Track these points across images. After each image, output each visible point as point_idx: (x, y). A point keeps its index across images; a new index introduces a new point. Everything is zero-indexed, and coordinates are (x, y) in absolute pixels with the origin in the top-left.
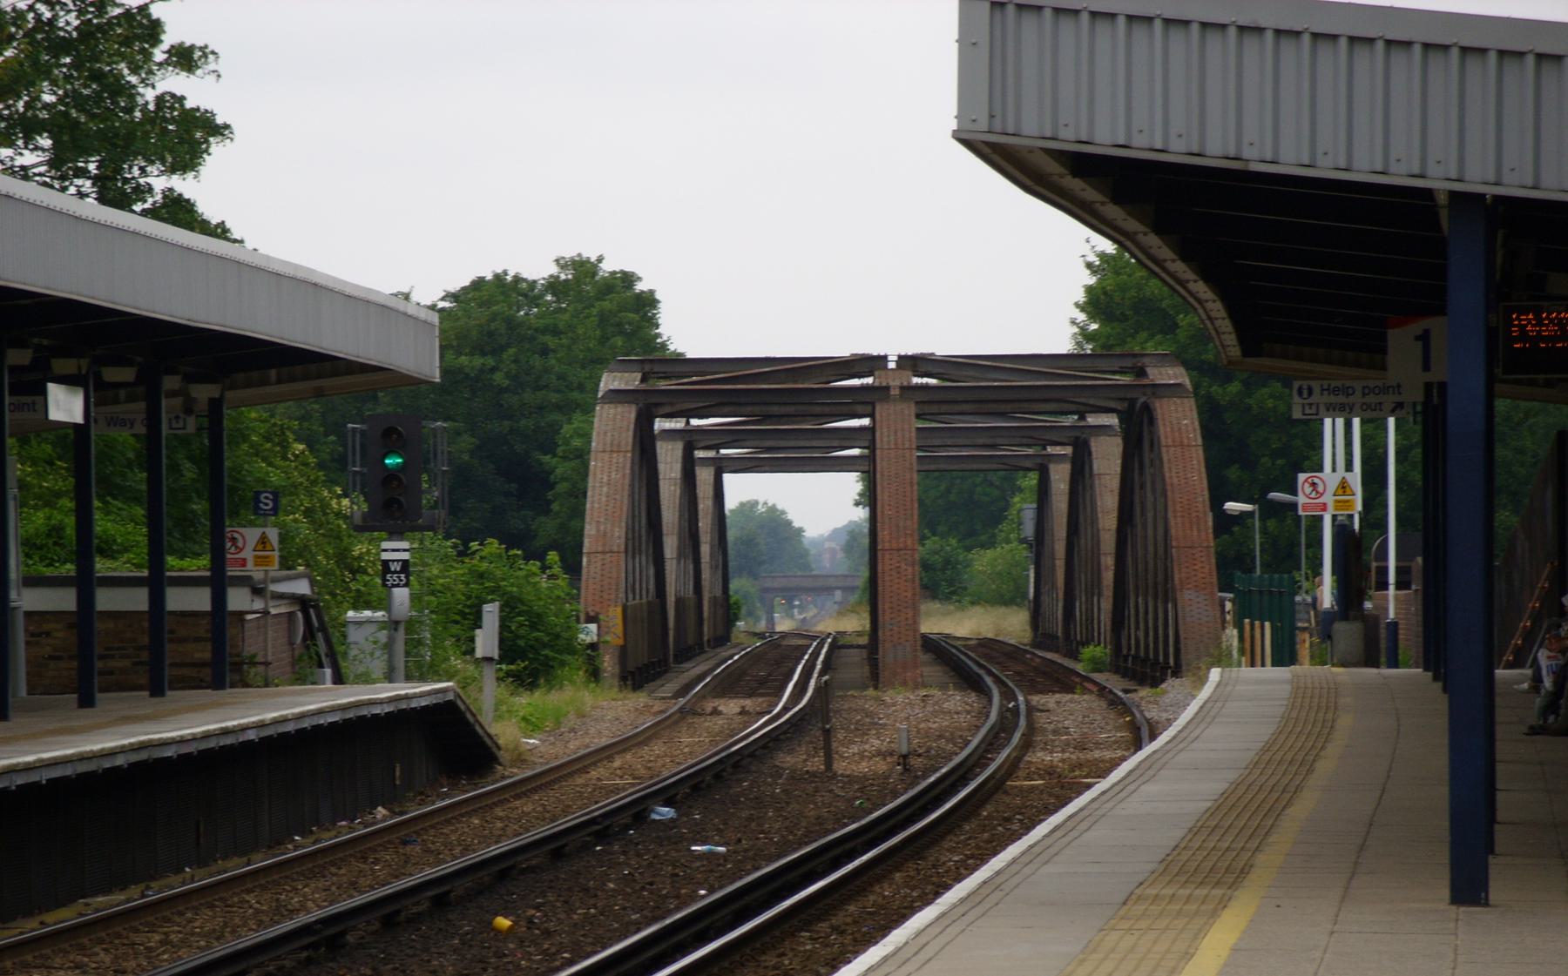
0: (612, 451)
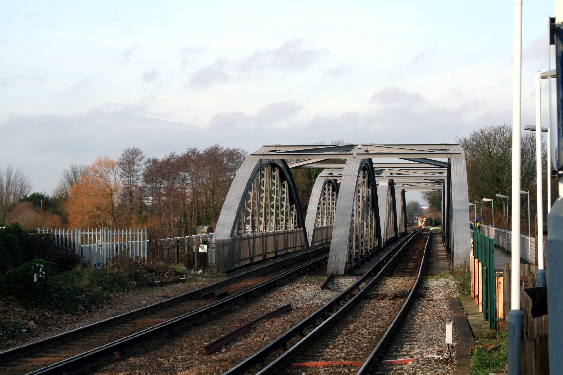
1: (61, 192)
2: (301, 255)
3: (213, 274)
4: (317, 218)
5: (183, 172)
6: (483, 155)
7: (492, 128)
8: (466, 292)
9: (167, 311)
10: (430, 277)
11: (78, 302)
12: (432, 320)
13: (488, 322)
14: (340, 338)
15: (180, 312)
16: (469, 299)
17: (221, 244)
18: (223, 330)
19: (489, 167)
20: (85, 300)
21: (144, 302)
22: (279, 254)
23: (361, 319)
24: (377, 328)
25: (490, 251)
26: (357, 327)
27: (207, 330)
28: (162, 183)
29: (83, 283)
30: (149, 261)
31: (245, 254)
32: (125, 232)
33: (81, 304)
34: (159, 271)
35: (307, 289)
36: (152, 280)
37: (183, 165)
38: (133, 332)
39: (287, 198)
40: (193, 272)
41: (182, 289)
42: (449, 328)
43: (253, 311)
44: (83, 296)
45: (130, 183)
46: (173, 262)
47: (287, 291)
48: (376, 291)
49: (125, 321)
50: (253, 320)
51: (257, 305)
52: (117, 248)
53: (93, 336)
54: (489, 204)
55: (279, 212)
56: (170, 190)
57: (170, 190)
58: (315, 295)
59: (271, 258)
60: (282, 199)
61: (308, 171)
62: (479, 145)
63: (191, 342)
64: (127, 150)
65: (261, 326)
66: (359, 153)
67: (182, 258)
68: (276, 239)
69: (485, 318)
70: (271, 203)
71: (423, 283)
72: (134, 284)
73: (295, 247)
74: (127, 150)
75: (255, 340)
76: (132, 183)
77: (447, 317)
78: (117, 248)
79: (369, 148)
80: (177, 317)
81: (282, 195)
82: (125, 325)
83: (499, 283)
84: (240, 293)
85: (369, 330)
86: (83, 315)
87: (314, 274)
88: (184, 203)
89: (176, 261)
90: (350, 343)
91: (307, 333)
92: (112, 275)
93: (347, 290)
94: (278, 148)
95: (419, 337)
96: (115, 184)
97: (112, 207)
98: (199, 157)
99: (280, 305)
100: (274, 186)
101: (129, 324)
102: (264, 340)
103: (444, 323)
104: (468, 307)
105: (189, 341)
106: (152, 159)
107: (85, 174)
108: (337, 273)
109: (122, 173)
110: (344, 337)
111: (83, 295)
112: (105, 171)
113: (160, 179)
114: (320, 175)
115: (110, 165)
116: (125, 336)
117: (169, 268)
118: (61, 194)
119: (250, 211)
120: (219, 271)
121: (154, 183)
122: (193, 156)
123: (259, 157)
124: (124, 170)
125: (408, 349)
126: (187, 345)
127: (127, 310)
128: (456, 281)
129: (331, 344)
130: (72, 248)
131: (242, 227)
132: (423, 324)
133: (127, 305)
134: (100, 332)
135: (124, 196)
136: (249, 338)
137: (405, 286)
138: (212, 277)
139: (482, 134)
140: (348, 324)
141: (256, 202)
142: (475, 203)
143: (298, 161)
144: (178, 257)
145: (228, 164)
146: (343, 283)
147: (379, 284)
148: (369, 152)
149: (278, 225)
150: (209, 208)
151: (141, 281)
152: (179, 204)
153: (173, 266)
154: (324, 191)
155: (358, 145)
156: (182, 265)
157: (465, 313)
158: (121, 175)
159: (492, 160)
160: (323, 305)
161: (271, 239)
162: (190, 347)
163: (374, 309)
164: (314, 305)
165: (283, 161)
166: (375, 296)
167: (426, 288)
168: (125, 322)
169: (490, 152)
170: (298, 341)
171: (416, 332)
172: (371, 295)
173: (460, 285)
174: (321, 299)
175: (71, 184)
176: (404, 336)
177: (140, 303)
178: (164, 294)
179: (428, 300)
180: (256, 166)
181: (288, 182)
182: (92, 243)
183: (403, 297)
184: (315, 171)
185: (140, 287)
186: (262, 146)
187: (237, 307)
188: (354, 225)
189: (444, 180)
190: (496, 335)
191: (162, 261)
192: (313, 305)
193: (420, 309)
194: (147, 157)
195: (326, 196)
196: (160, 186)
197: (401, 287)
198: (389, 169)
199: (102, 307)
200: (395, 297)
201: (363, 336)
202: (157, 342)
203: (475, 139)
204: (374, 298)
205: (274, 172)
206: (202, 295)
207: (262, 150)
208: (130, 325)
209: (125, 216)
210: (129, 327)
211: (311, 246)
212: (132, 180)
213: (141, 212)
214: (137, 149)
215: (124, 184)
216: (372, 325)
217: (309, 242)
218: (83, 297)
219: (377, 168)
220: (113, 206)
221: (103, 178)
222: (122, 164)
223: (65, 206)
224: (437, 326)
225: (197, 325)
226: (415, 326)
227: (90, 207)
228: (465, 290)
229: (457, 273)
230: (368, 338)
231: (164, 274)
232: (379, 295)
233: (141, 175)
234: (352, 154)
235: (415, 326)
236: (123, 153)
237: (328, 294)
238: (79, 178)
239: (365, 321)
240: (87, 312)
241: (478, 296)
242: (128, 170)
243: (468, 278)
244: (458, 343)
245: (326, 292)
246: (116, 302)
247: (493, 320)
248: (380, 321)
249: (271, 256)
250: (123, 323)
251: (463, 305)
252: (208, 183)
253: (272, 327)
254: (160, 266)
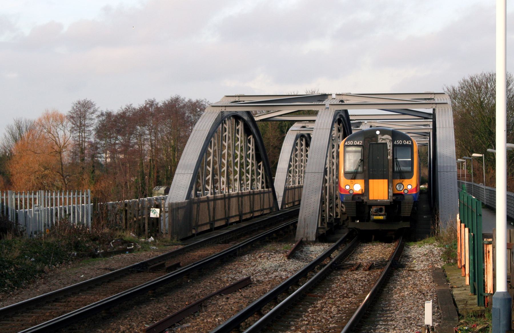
1: (4, 150)
2: (268, 219)
3: (166, 241)
4: (288, 176)
5: (140, 126)
6: (473, 105)
7: (483, 75)
8: (452, 261)
9: (108, 286)
10: (412, 243)
11: (6, 277)
12: (412, 295)
13: (476, 297)
14: (304, 318)
15: (123, 287)
16: (455, 269)
17: (175, 208)
18: (168, 309)
19: (480, 119)
20: (14, 274)
21: (83, 276)
22: (244, 218)
23: (330, 294)
24: (348, 305)
25: (477, 215)
26: (325, 304)
27: (151, 309)
28: (117, 139)
29: (13, 255)
30: (92, 228)
31: (204, 218)
32: (62, 195)
33: (9, 279)
34: (103, 238)
35: (271, 258)
36: (96, 249)
37: (140, 119)
38: (64, 312)
39: (253, 155)
40: (143, 240)
41: (128, 260)
42: (429, 306)
43: (207, 286)
44: (12, 269)
45: (81, 139)
46: (120, 229)
47: (248, 261)
48: (350, 260)
49: (56, 299)
50: (206, 296)
51: (212, 278)
52: (57, 213)
53: (16, 318)
54: (480, 160)
55: (244, 171)
56: (126, 146)
57: (126, 146)
58: (280, 266)
59: (234, 222)
60: (248, 156)
61: (280, 124)
62: (469, 95)
63: (130, 325)
64: (77, 102)
65: (213, 304)
66: (332, 103)
67: (130, 224)
68: (240, 201)
69: (473, 292)
70: (234, 160)
71: (404, 251)
72: (74, 254)
73: (262, 210)
74: (77, 102)
75: (205, 321)
76: (83, 139)
77: (428, 291)
78: (57, 213)
79: (344, 98)
80: (118, 293)
81: (247, 152)
82: (57, 303)
83: (487, 252)
84: (194, 264)
85: (339, 307)
86: (11, 291)
87: (280, 241)
88: (142, 160)
89: (124, 227)
90: (315, 323)
91: (266, 311)
92: (48, 244)
93: (317, 259)
94: (241, 99)
95: (396, 315)
96: (65, 141)
97: (61, 166)
98: (158, 110)
99: (239, 277)
100: (238, 141)
101: (61, 302)
102: (216, 321)
103: (425, 298)
104: (453, 279)
105: (127, 323)
106: (106, 112)
107: (31, 129)
108: (307, 239)
109: (73, 128)
110: (309, 316)
111: (12, 268)
112: (54, 126)
113: (115, 135)
114: (291, 128)
115: (59, 119)
116: (54, 317)
117: (116, 235)
118: (4, 151)
119: (210, 169)
120: (172, 238)
121: (109, 138)
122: (152, 108)
123: (220, 108)
124: (74, 124)
125: (382, 330)
126: (124, 328)
127: (62, 286)
128: (441, 248)
129: (293, 325)
130: (5, 213)
131: (201, 188)
132: (401, 300)
133: (63, 279)
134: (25, 312)
135: (75, 153)
136: (199, 318)
137: (383, 254)
138: (165, 245)
139: (472, 82)
140: (315, 300)
141: (217, 159)
142: (464, 159)
143: (268, 112)
144: (126, 223)
145: (190, 117)
146: (313, 251)
147: (354, 252)
148: (344, 102)
149: (231, 185)
150: (169, 166)
151: (82, 251)
152: (136, 162)
153: (119, 233)
154: (296, 147)
155: (331, 95)
156: (130, 232)
157: (450, 286)
158: (71, 130)
159: (483, 111)
160: (288, 277)
161: (234, 201)
162: (127, 331)
163: (346, 282)
164: (277, 278)
165: (248, 113)
166: (348, 266)
167: (407, 257)
168: (56, 300)
169: (482, 102)
170: (255, 322)
171: (392, 310)
172: (343, 265)
173: (445, 252)
174: (286, 271)
175: (16, 140)
176: (378, 315)
177: (78, 277)
178: (107, 266)
179: (409, 271)
180: (216, 119)
181: (254, 137)
182: (63, 205)
183: (381, 267)
184: (287, 125)
185: (80, 257)
186: (223, 96)
187: (189, 281)
188: (327, 185)
189: (429, 133)
190: (485, 313)
191: (107, 227)
192: (276, 278)
193: (398, 281)
194: (100, 110)
195: (298, 152)
196: (115, 142)
197: (379, 255)
198: (368, 121)
199: (34, 282)
200: (371, 267)
201: (331, 314)
202: (89, 325)
203: (464, 87)
204: (348, 268)
205: (237, 126)
206: (150, 267)
207: (224, 100)
208: (61, 304)
209: (75, 176)
210: (60, 306)
211: (281, 208)
212: (83, 135)
213: (93, 171)
214: (88, 102)
215: (75, 140)
216: (342, 301)
217: (278, 204)
218: (12, 271)
219: (353, 120)
220: (62, 165)
221: (51, 133)
222: (72, 117)
223: (8, 165)
224: (417, 302)
225: (139, 303)
226: (392, 302)
227: (37, 166)
228: (450, 258)
229: (442, 238)
230: (337, 317)
231: (109, 242)
232: (352, 265)
233: (93, 130)
234: (325, 105)
235: (392, 302)
236: (72, 105)
237: (295, 264)
238: (25, 134)
239: (335, 296)
240: (16, 287)
241: (464, 266)
242: (78, 124)
243: (455, 245)
244: (440, 322)
245: (292, 261)
246: (51, 276)
247: (481, 295)
248: (353, 296)
249: (235, 221)
250: (54, 301)
251: (448, 276)
252: (168, 138)
253: (226, 305)
254: (105, 233)
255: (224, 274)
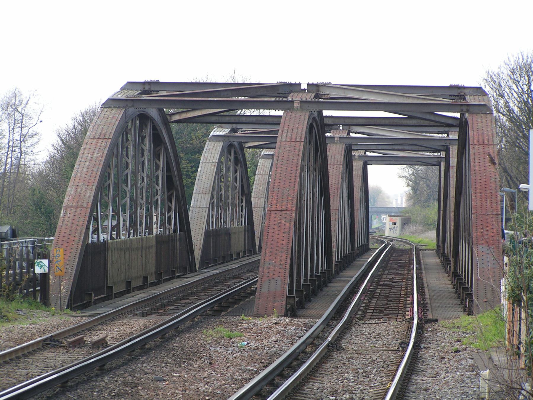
0: (99, 138)
255: (410, 181)
